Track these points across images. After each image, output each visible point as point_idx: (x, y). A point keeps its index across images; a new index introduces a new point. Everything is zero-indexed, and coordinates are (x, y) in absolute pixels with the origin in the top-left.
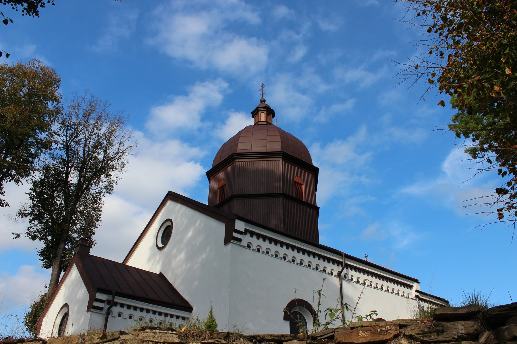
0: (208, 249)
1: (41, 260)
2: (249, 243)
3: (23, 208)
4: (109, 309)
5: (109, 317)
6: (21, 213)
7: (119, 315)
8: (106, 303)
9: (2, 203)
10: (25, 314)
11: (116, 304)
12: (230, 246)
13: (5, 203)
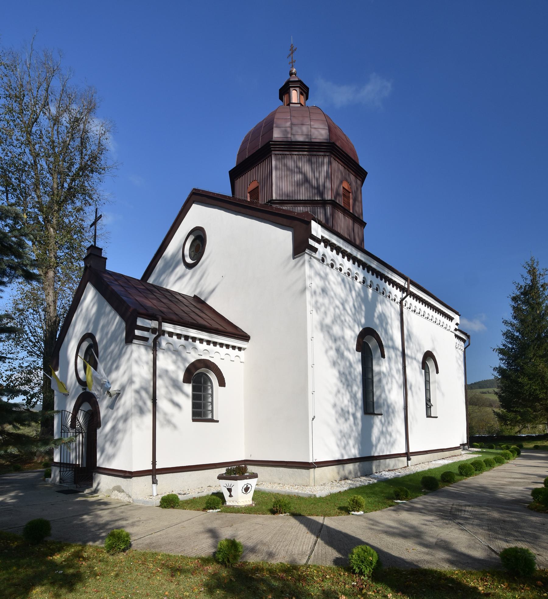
4: (155, 340)
8: (150, 331)
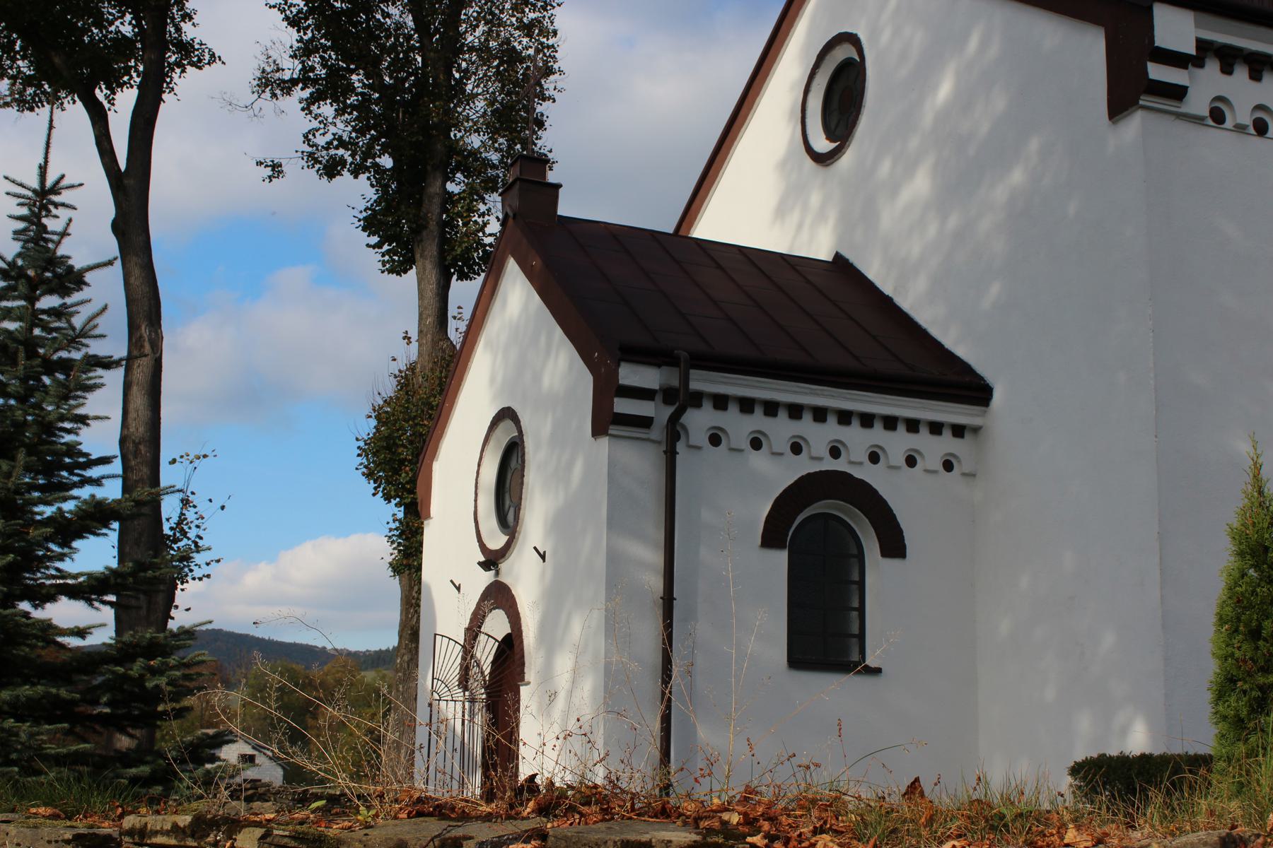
0: (1034, 145)
1: (374, 247)
2: (1219, 99)
3: (270, 60)
4: (674, 420)
5: (677, 450)
6: (267, 79)
7: (715, 440)
8: (659, 397)
9: (196, 53)
10: (357, 439)
11: (696, 399)
12: (1135, 123)
13: (207, 51)
